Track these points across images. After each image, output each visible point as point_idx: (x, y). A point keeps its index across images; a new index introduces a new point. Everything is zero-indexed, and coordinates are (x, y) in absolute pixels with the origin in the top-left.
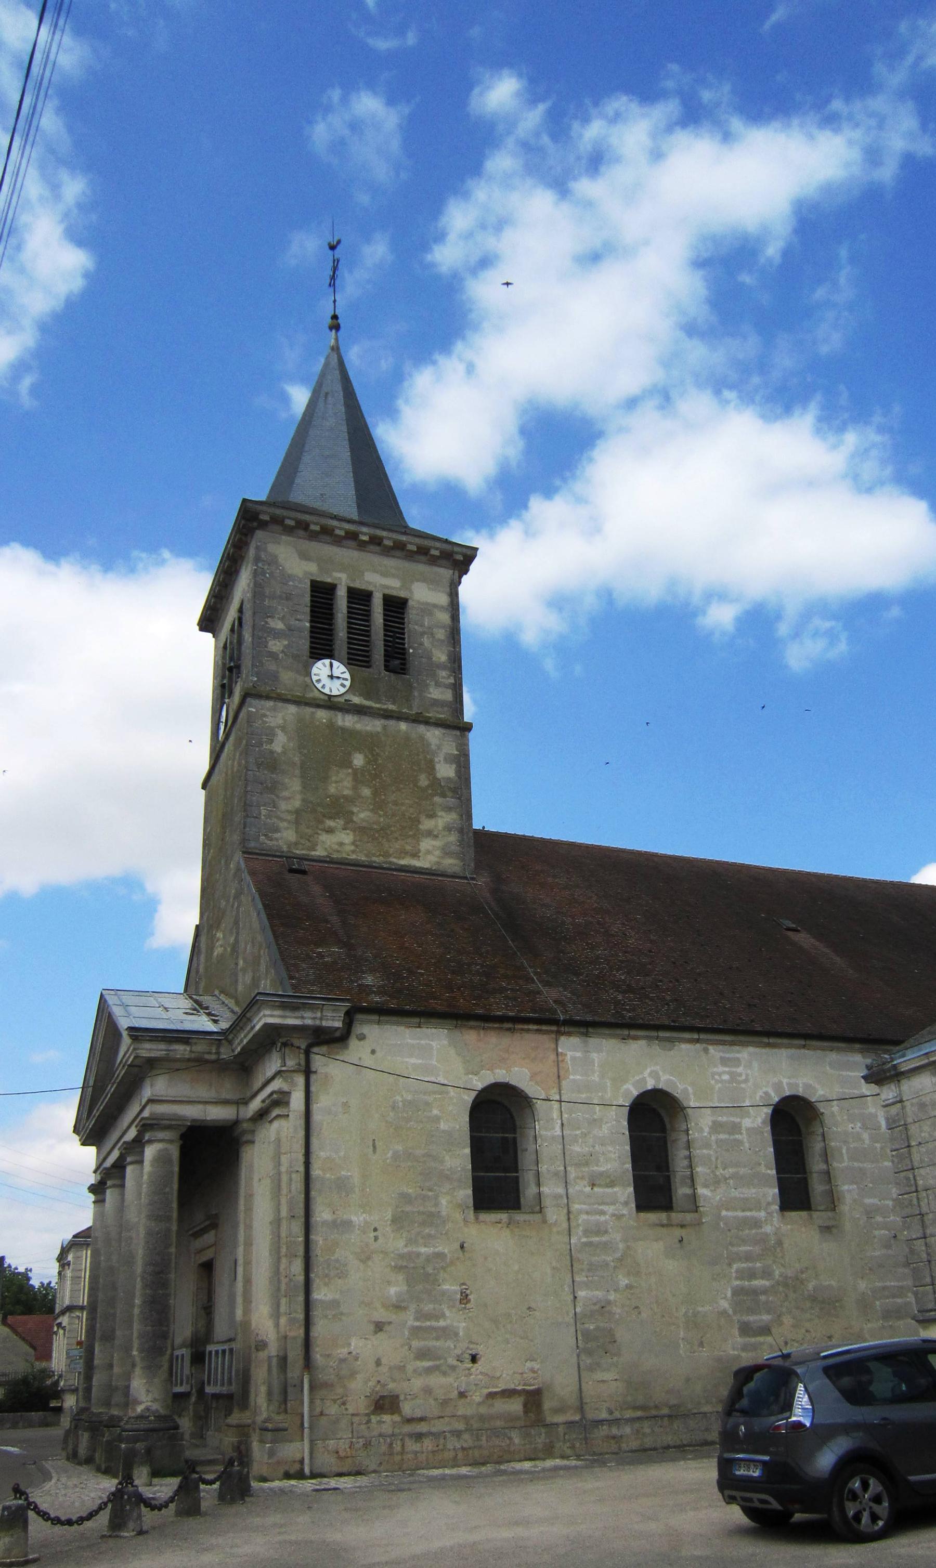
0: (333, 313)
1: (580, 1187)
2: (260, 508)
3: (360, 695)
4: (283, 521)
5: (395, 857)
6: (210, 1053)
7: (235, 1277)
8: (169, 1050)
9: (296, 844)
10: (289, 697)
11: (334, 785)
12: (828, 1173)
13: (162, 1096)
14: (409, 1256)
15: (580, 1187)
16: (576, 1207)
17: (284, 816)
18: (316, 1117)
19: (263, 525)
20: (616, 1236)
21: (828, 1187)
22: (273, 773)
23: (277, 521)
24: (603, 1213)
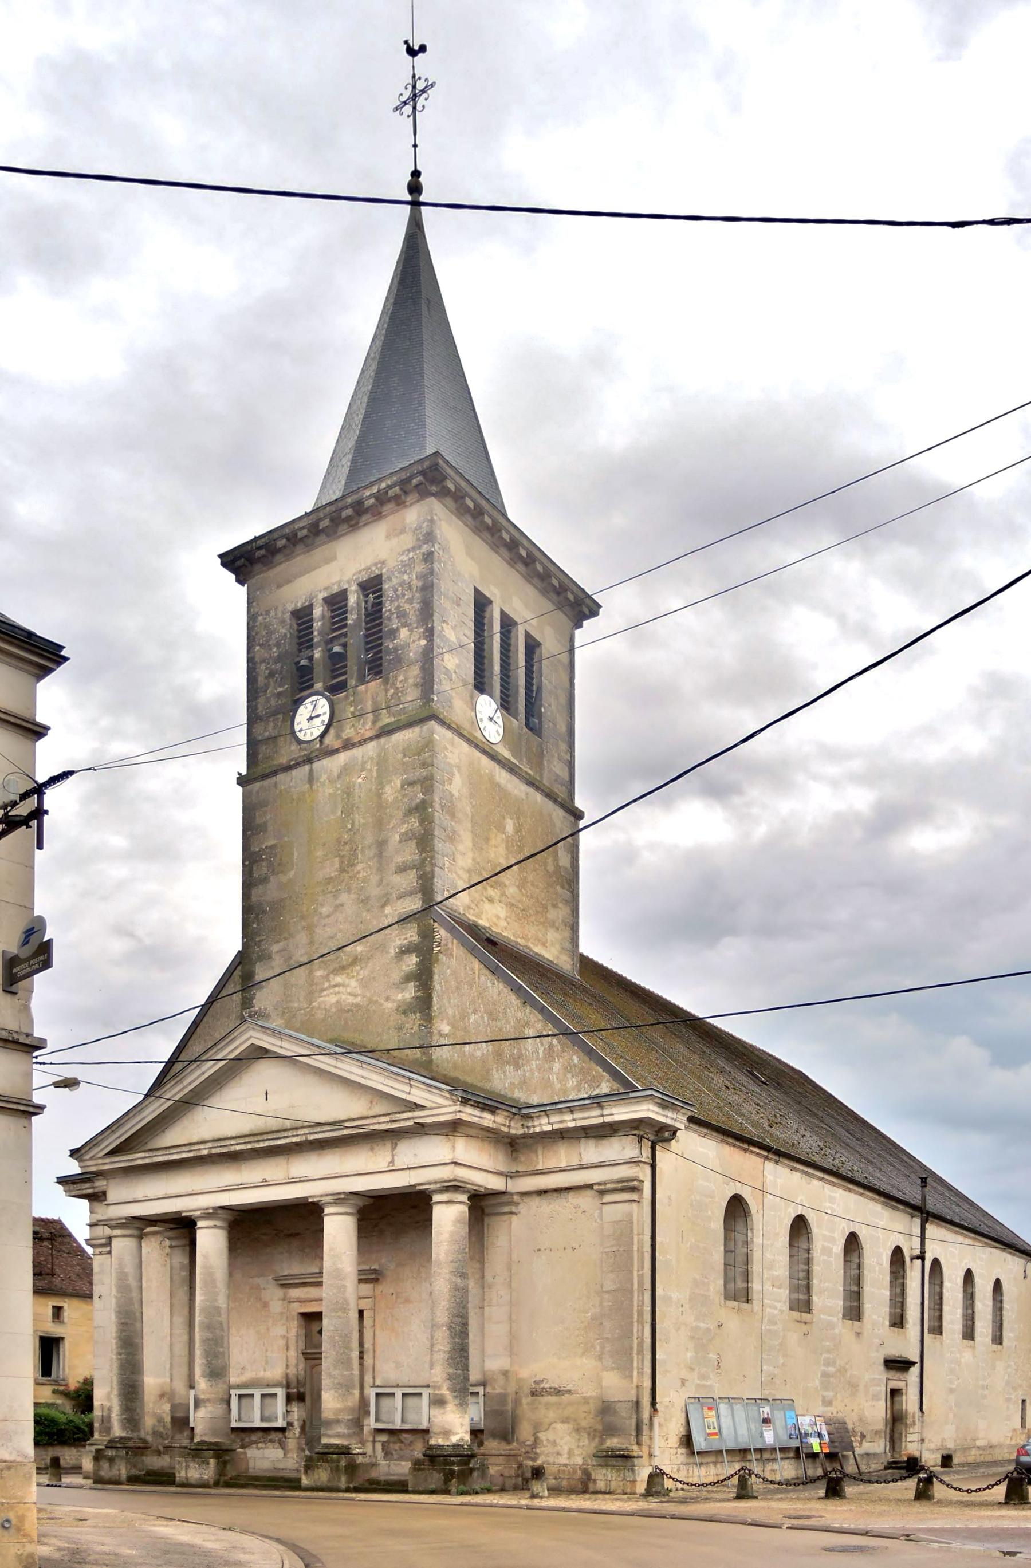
0: (413, 169)
1: (768, 1286)
2: (450, 471)
3: (509, 750)
4: (463, 498)
5: (532, 943)
6: (504, 1125)
7: (171, 1350)
8: (480, 1117)
9: (469, 908)
10: (465, 733)
11: (493, 849)
12: (859, 1293)
13: (821, 1179)
14: (696, 1329)
15: (768, 1286)
16: (766, 1301)
17: (460, 872)
18: (572, 1198)
19: (443, 493)
20: (779, 1327)
21: (855, 1304)
22: (452, 820)
23: (458, 497)
24: (776, 1308)
